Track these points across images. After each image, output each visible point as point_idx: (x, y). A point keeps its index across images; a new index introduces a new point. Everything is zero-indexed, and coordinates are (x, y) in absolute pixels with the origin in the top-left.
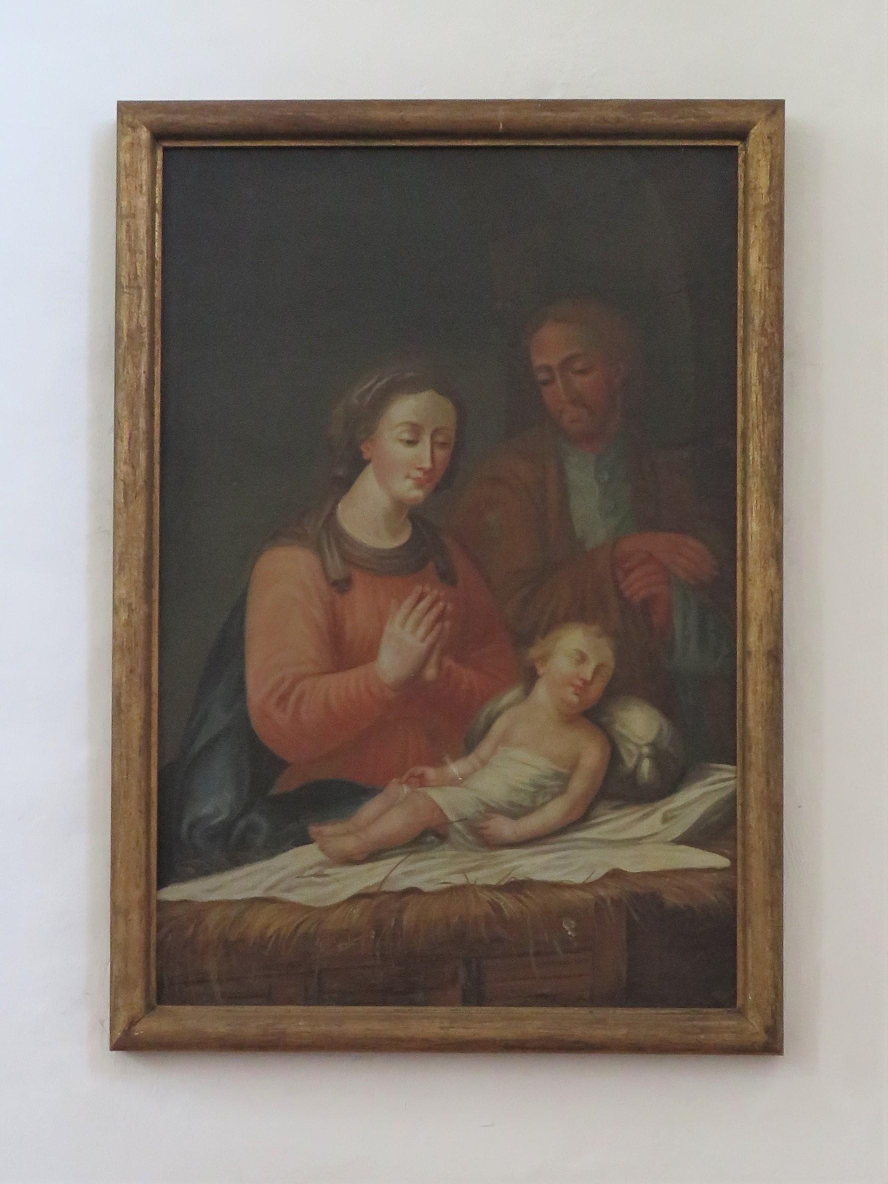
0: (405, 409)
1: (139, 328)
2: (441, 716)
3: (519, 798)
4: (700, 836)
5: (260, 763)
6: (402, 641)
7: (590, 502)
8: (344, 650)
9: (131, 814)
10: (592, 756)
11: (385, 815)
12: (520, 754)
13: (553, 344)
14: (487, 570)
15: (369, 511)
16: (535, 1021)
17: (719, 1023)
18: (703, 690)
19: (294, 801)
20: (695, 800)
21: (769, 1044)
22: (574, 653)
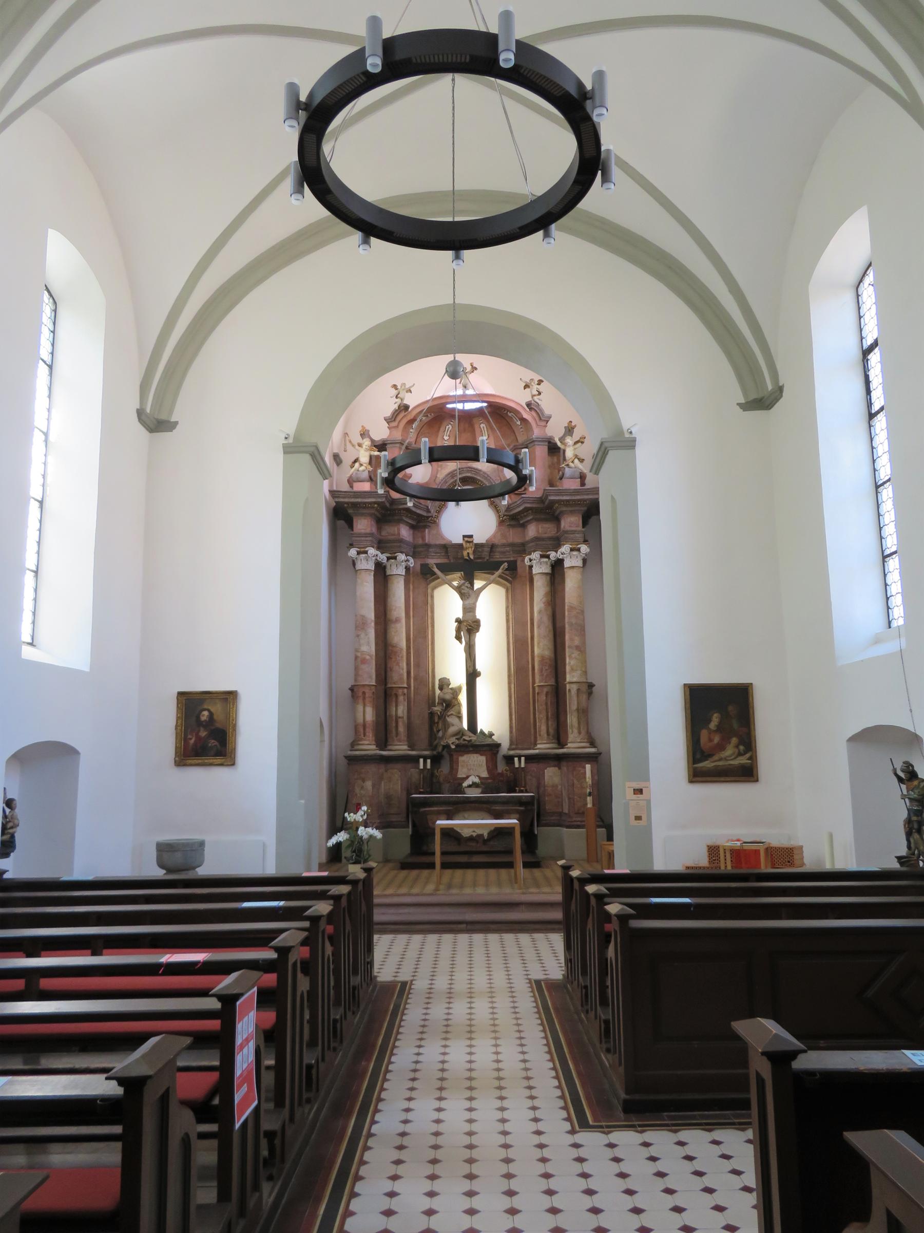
0: (715, 715)
1: (360, 625)
2: (721, 747)
3: (730, 755)
4: (748, 759)
5: (702, 752)
6: (717, 739)
7: (735, 725)
8: (711, 740)
9: (523, 480)
10: (737, 751)
11: (716, 757)
12: (729, 751)
13: (730, 708)
14: (725, 731)
15: (713, 725)
16: (733, 779)
17: (752, 779)
18: (748, 743)
19: (706, 756)
20: (748, 755)
21: (757, 781)
22: (734, 740)
